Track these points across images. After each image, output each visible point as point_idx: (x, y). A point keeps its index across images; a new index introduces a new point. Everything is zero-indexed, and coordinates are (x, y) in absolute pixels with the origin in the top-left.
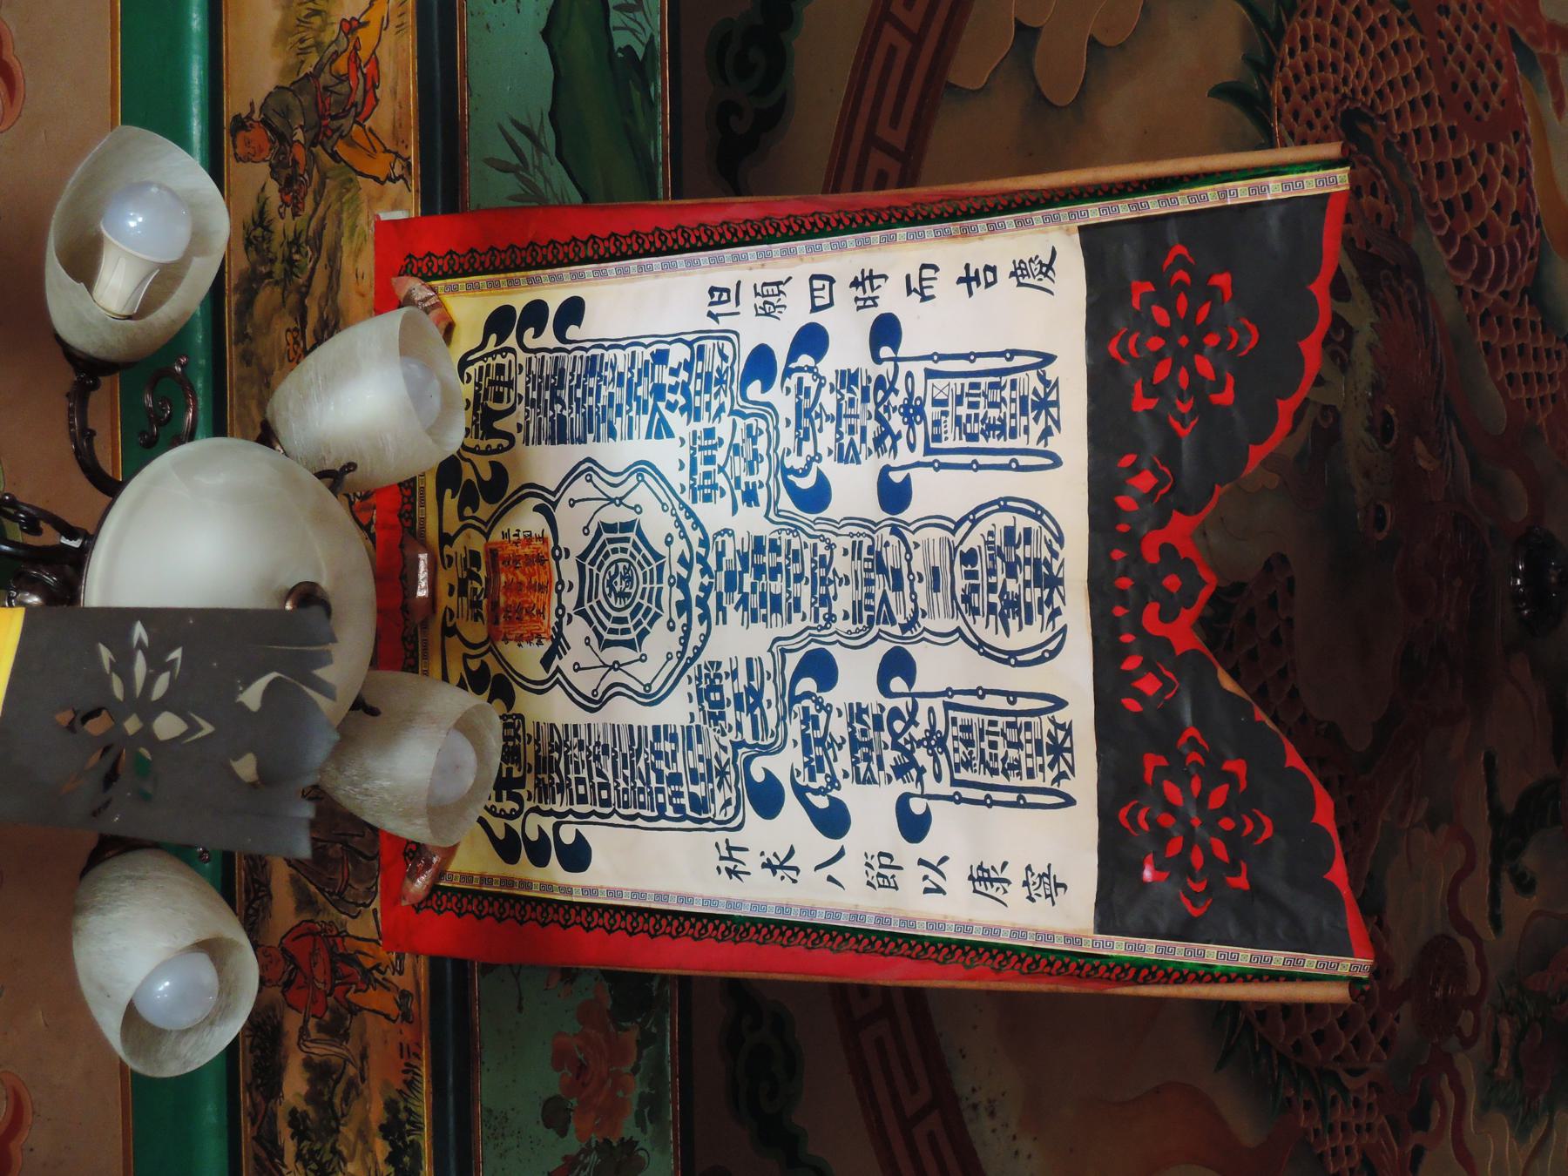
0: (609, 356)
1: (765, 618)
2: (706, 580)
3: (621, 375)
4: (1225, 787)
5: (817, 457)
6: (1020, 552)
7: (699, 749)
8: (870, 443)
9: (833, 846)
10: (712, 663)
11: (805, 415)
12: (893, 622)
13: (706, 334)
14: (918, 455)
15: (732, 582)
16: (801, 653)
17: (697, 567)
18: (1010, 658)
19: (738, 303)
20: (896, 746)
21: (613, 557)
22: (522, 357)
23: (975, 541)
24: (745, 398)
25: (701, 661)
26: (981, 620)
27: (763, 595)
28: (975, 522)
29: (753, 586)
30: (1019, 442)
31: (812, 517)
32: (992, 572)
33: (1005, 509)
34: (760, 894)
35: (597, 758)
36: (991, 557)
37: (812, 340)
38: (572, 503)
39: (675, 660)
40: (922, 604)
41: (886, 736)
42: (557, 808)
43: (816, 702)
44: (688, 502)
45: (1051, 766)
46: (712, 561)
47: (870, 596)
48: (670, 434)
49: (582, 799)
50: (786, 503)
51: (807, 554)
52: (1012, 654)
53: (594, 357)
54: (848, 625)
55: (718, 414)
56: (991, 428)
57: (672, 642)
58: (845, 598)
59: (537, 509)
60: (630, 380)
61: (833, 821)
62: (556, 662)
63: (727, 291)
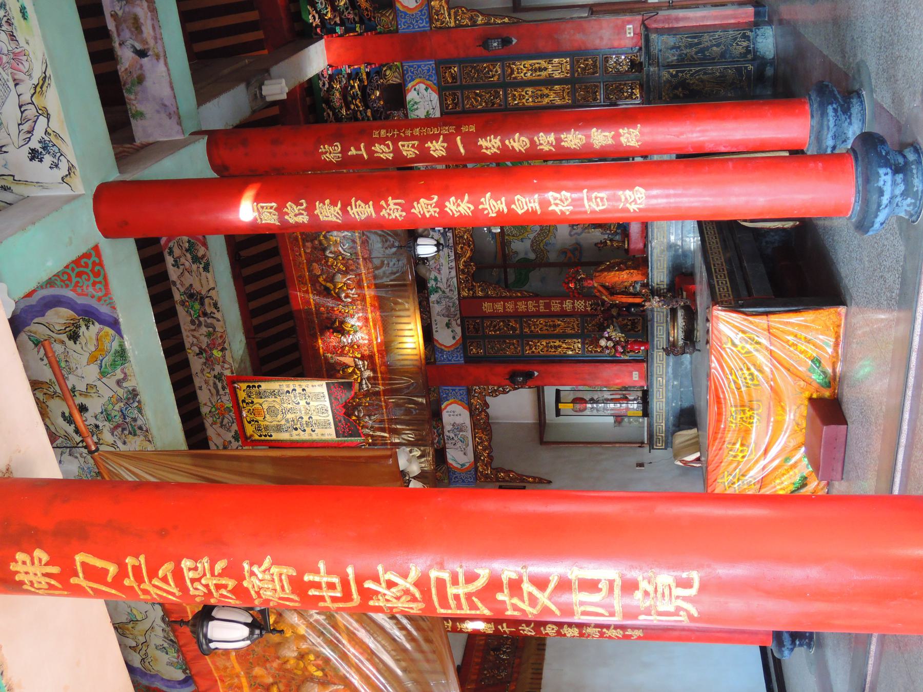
37: (294, 390)
61: (304, 431)
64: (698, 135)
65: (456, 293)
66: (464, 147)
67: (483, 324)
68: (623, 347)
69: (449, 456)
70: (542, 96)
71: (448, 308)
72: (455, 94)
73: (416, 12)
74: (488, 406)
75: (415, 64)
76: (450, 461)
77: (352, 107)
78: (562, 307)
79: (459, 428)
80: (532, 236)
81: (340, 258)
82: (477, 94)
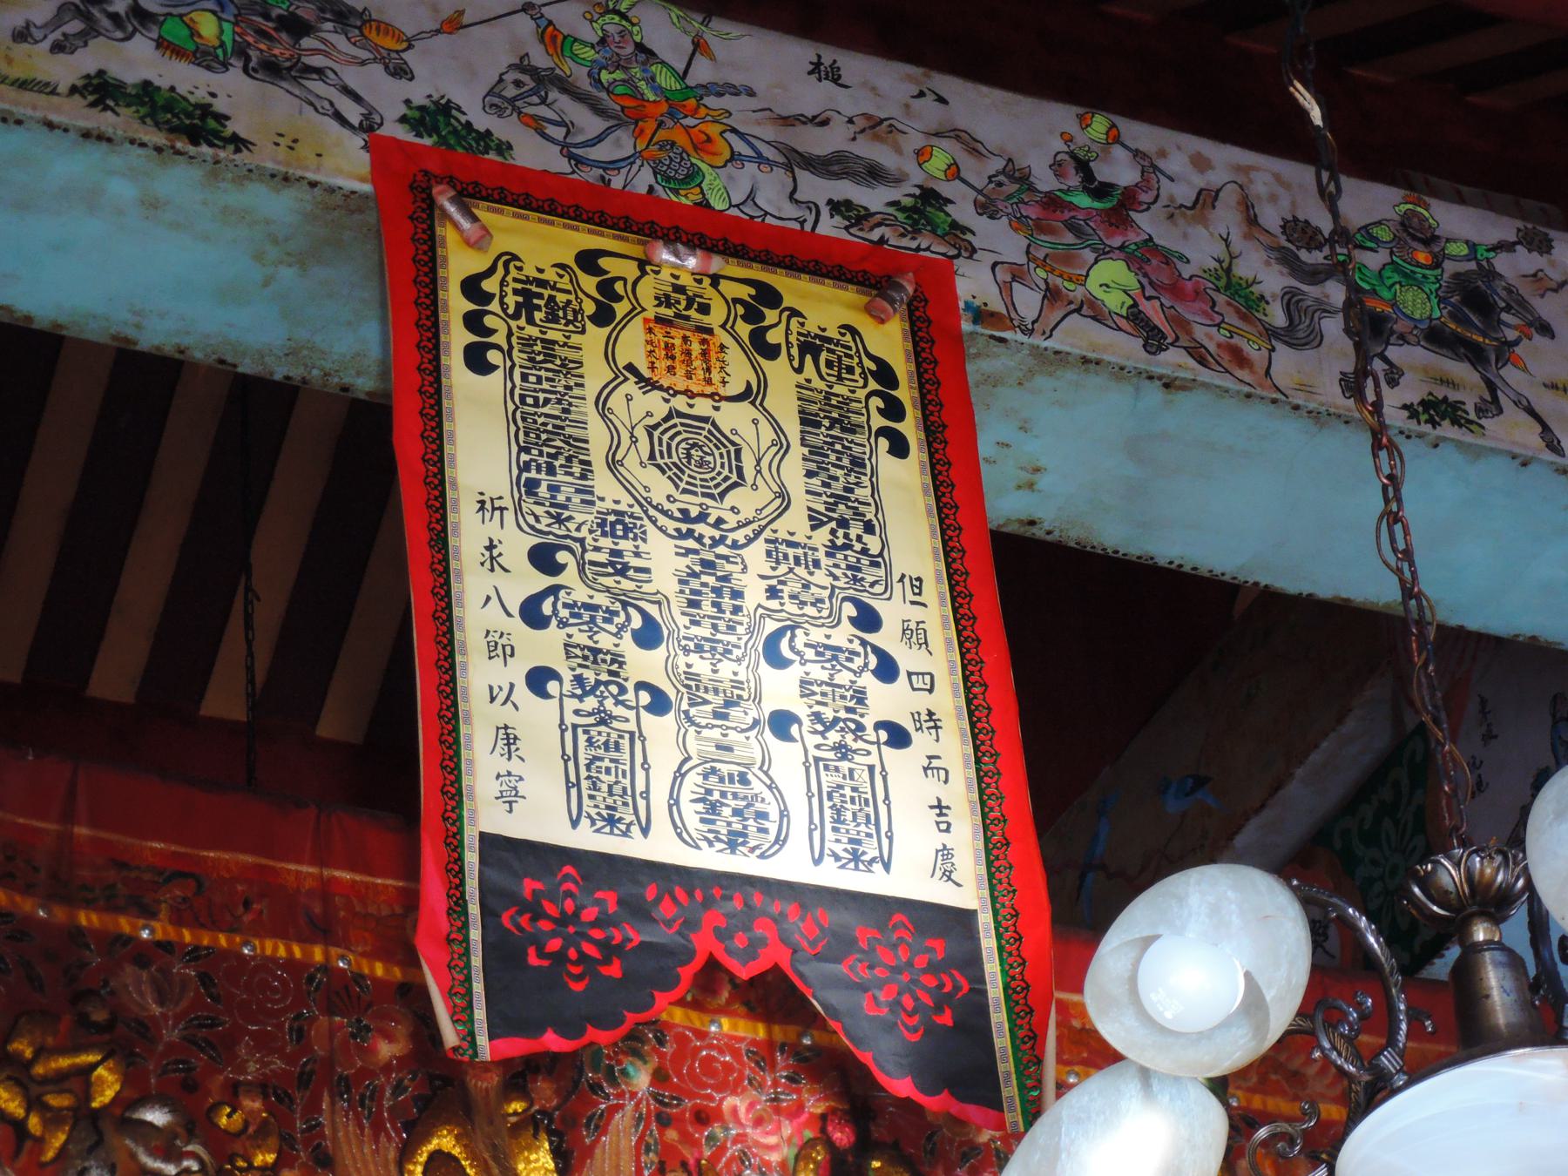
0: (865, 480)
1: (682, 592)
2: (707, 541)
3: (851, 491)
4: (597, 956)
5: (804, 662)
6: (751, 822)
7: (576, 499)
8: (817, 708)
9: (514, 608)
10: (644, 533)
12: (691, 705)
13: (888, 573)
14: (813, 752)
15: (708, 565)
16: (659, 620)
17: (717, 534)
18: (674, 802)
19: (913, 603)
20: (598, 683)
21: (717, 453)
22: (861, 394)
23: (757, 786)
24: (844, 599)
25: (646, 522)
26: (700, 780)
27: (698, 593)
28: (770, 787)
29: (704, 585)
30: (829, 835)
31: (760, 649)
32: (735, 796)
33: (782, 816)
34: (469, 533)
35: (559, 402)
36: (745, 798)
37: (887, 669)
38: (755, 422)
39: (645, 495)
40: (706, 733)
41: (604, 677)
42: (515, 353)
43: (623, 626)
44: (765, 535)
45: (599, 814)
46: (722, 550)
47: (706, 690)
48: (813, 528)
49: (524, 377)
50: (771, 626)
51: (733, 639)
52: (677, 802)
53: (864, 466)
54: (683, 668)
55: (831, 574)
56: (838, 811)
57: (658, 497)
58: (701, 666)
59: (749, 384)
60: (848, 499)
61: (532, 613)
62: (633, 379)
63: (920, 594)
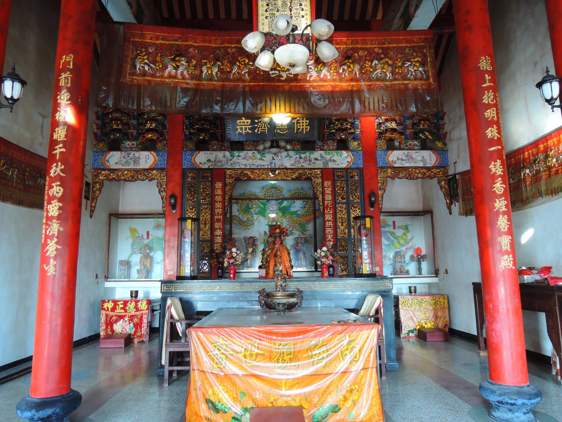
11: (297, 9)
37: (303, 10)
61: (266, 11)
64: (505, 307)
65: (230, 167)
66: (495, 150)
67: (208, 182)
68: (232, 263)
69: (115, 153)
70: (342, 223)
71: (220, 161)
72: (344, 177)
73: (387, 161)
74: (150, 180)
75: (361, 157)
76: (111, 153)
77: (337, 123)
78: (217, 229)
79: (136, 161)
80: (240, 216)
81: (371, 70)
82: (343, 188)
